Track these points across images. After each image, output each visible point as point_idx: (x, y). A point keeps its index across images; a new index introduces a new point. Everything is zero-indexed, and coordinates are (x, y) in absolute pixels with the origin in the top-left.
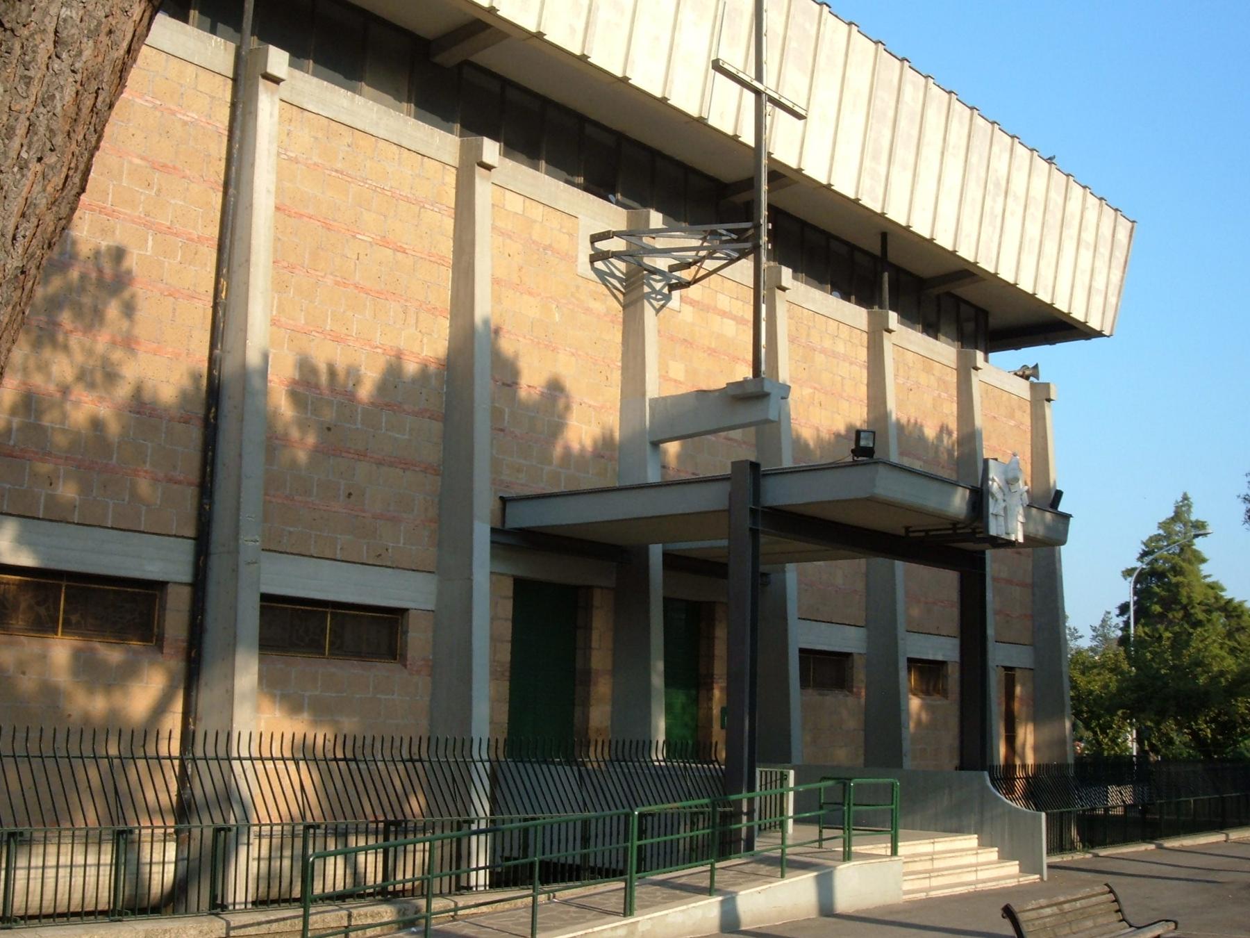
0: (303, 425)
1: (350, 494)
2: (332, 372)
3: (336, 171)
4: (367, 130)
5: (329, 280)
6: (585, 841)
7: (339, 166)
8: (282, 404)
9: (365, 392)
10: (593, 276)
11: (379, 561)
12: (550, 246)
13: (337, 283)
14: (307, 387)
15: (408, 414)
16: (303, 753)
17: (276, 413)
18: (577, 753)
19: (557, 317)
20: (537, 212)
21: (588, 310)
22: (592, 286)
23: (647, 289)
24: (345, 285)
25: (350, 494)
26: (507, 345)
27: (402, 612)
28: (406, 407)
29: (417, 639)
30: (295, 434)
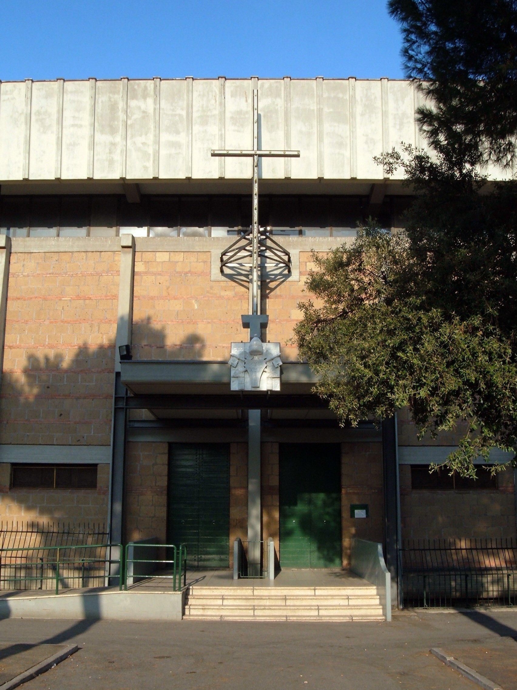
0: (31, 385)
1: (61, 415)
2: (47, 359)
3: (50, 274)
4: (66, 251)
5: (47, 322)
6: (104, 534)
7: (51, 271)
8: (23, 379)
9: (65, 364)
10: (224, 278)
11: (79, 443)
12: (190, 271)
13: (51, 323)
14: (33, 369)
15: (94, 373)
16: (34, 527)
17: (17, 381)
18: (233, 482)
19: (196, 307)
20: (180, 257)
21: (221, 297)
22: (223, 284)
23: (268, 281)
24: (56, 322)
25: (61, 415)
26: (156, 325)
27: (96, 465)
28: (93, 370)
29: (104, 477)
30: (27, 389)
